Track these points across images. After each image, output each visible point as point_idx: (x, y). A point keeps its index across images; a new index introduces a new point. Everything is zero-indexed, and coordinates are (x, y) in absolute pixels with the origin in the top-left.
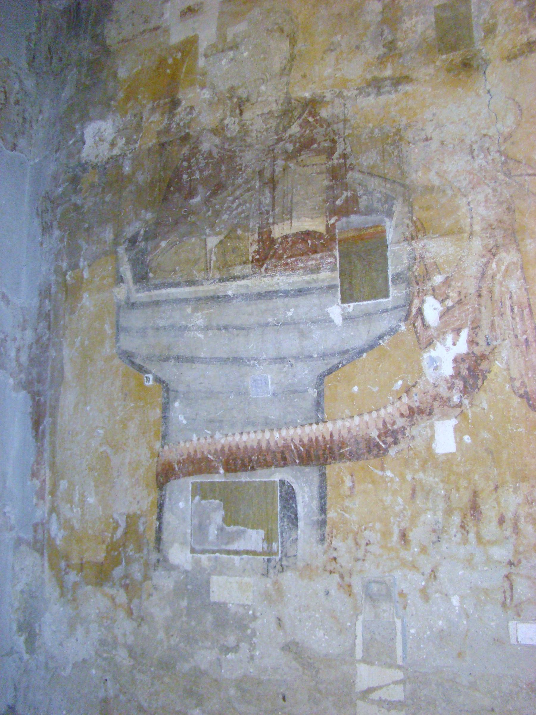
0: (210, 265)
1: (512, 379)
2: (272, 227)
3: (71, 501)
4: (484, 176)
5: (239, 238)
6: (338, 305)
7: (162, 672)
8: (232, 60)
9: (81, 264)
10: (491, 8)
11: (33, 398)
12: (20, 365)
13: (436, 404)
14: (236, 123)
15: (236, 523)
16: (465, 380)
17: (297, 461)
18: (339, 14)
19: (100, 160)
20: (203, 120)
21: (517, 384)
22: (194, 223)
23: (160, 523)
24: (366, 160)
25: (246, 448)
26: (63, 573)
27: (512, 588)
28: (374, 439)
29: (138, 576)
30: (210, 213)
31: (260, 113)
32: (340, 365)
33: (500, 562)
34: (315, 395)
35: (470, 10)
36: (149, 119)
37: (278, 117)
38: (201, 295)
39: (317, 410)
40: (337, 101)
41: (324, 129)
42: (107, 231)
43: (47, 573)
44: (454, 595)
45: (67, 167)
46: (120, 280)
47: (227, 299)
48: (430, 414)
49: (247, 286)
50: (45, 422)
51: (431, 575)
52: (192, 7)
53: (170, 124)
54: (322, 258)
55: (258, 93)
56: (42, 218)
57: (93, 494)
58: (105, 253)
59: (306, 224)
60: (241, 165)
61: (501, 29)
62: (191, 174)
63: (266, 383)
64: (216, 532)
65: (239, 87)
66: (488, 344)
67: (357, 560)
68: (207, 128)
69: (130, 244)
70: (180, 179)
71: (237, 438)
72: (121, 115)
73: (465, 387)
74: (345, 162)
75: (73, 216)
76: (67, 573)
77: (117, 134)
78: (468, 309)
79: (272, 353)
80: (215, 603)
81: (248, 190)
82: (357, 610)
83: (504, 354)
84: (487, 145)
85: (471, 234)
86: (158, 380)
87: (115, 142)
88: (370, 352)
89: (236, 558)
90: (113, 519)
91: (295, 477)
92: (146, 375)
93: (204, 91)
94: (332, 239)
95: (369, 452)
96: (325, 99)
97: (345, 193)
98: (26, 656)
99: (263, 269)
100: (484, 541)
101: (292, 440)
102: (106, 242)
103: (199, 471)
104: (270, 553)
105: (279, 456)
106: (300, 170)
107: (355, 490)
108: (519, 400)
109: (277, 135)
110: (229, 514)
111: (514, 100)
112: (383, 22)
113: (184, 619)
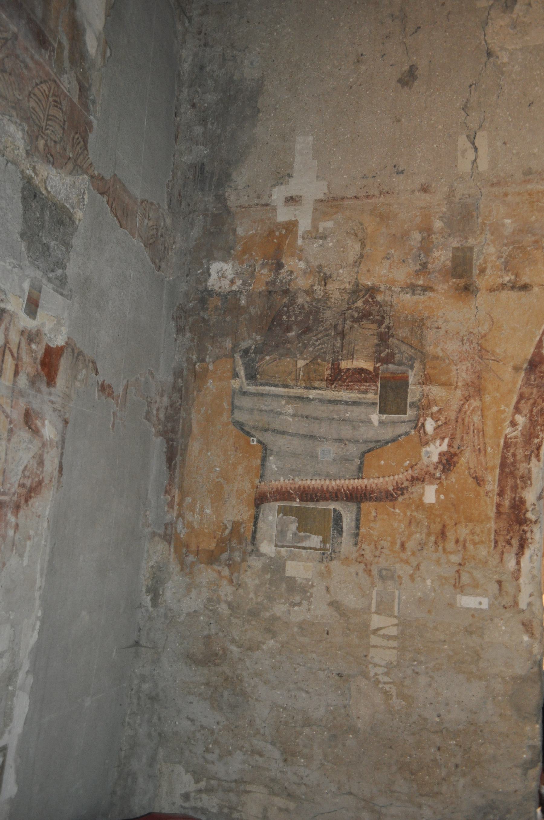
1: (469, 469)
2: (340, 362)
3: (193, 511)
4: (468, 356)
5: (318, 364)
7: (250, 618)
9: (207, 360)
11: (168, 442)
12: (159, 420)
13: (427, 476)
16: (444, 465)
20: (299, 282)
21: (472, 471)
22: (289, 349)
23: (256, 528)
24: (402, 333)
25: (314, 488)
27: (460, 577)
28: (390, 491)
29: (238, 559)
30: (300, 345)
33: (455, 563)
34: (359, 463)
36: (260, 271)
37: (349, 293)
38: (291, 394)
40: (387, 292)
42: (227, 341)
43: (172, 556)
46: (236, 375)
47: (309, 400)
48: (423, 481)
49: (322, 395)
54: (369, 386)
55: (338, 274)
57: (210, 507)
58: (226, 356)
60: (323, 318)
61: (488, 271)
62: (289, 317)
65: (325, 267)
67: (375, 556)
71: (309, 482)
73: (444, 469)
75: (201, 326)
76: (187, 556)
79: (335, 436)
80: (288, 577)
81: (327, 335)
82: (373, 584)
83: (467, 454)
84: (472, 338)
86: (259, 441)
90: (223, 523)
92: (252, 438)
93: (301, 262)
94: (377, 375)
95: (387, 498)
97: (387, 350)
98: (151, 609)
99: (333, 386)
101: (343, 487)
102: (226, 348)
104: (325, 549)
105: (334, 495)
106: (360, 330)
107: (378, 518)
112: (421, 248)
113: (267, 586)
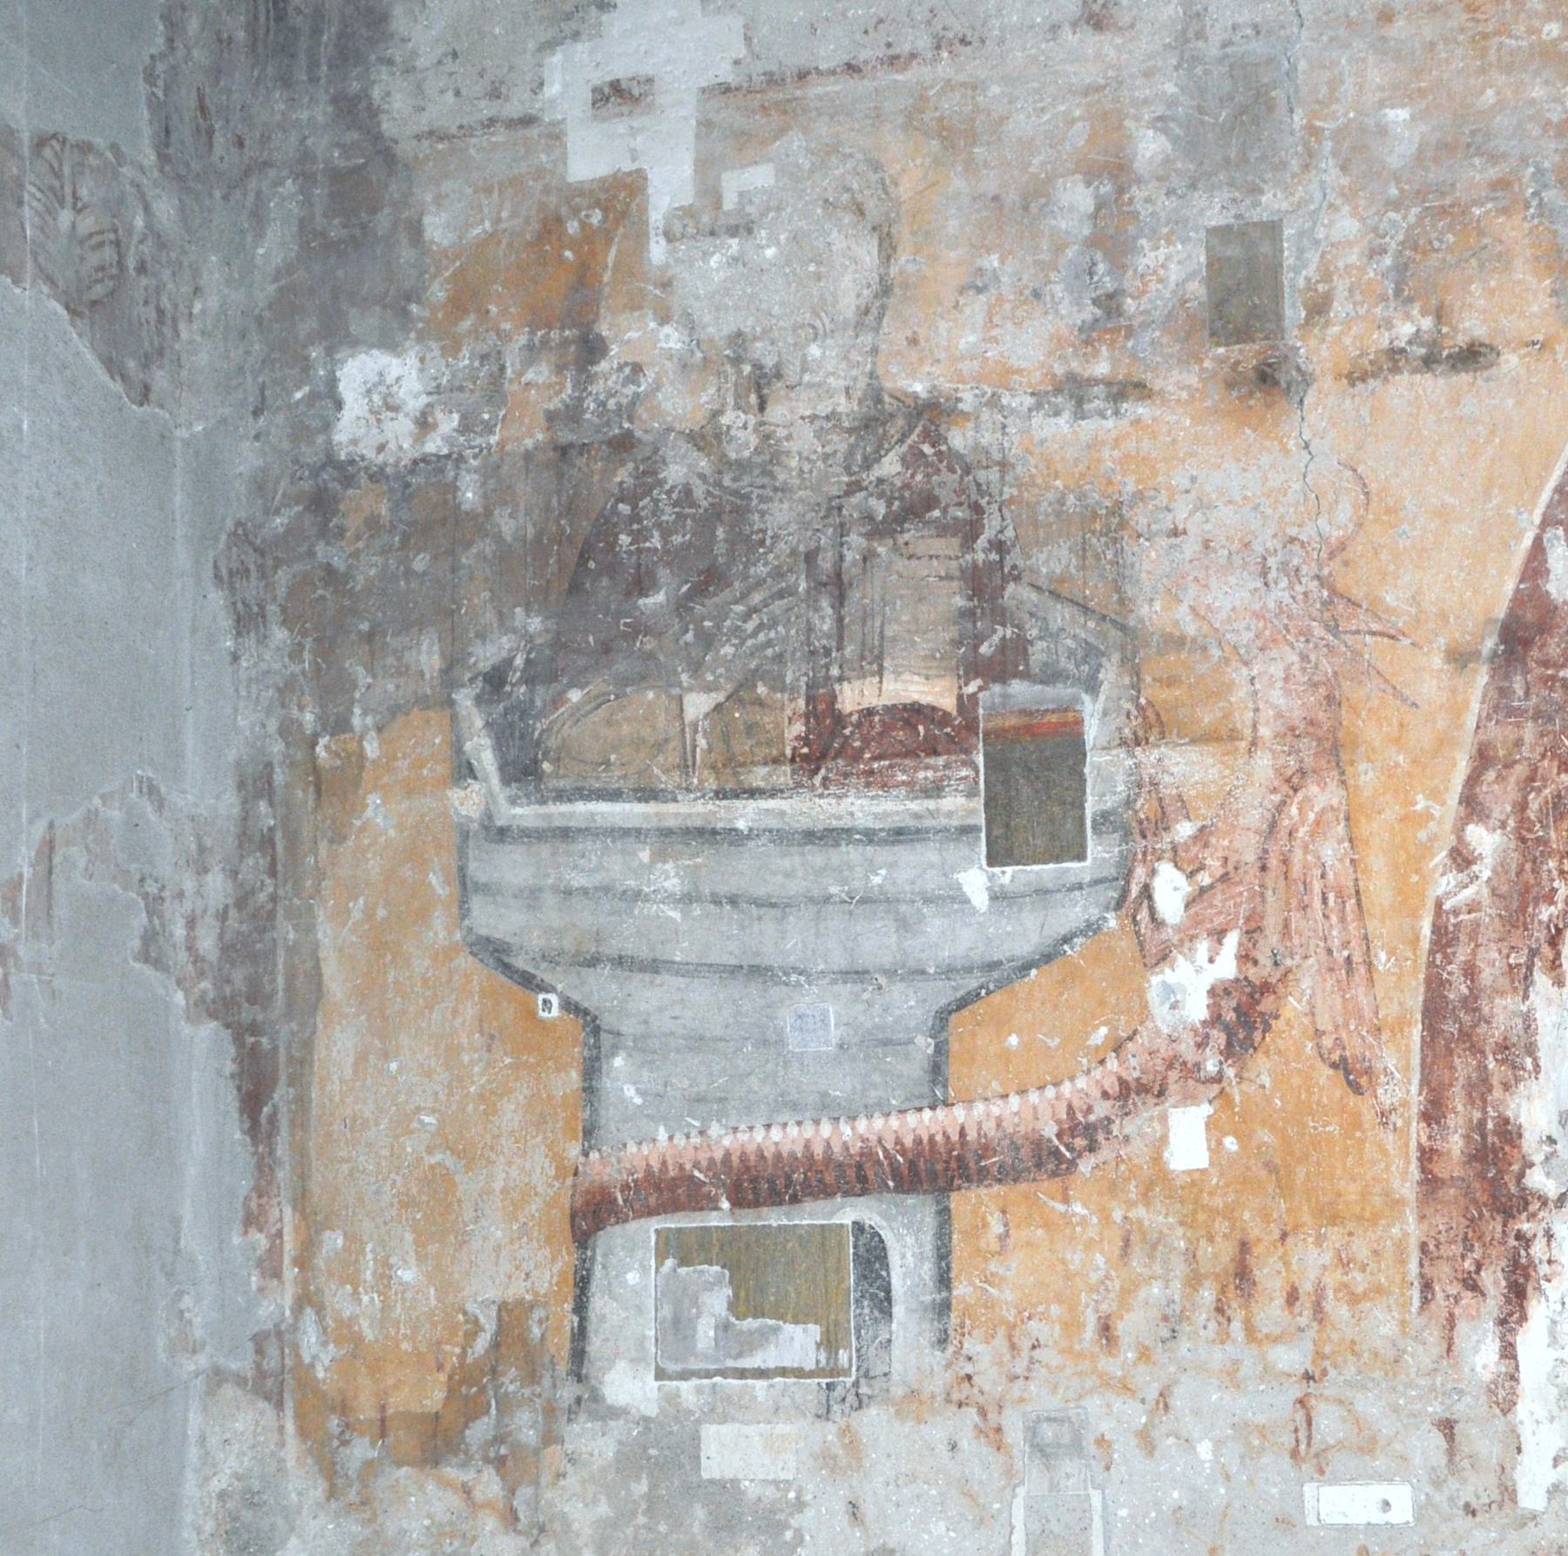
0: (694, 757)
1: (1318, 1034)
2: (837, 687)
4: (1286, 627)
5: (760, 703)
6: (981, 868)
8: (735, 259)
9: (356, 721)
10: (1322, 256)
11: (238, 1040)
12: (197, 959)
13: (1173, 1075)
14: (750, 427)
15: (758, 1313)
16: (1229, 1031)
17: (891, 1184)
18: (996, 198)
19: (391, 461)
20: (667, 406)
21: (1327, 1042)
22: (651, 656)
23: (583, 1320)
24: (1047, 561)
25: (778, 1156)
26: (336, 1443)
27: (1309, 1423)
28: (1049, 1140)
29: (530, 1436)
30: (689, 637)
31: (807, 413)
32: (983, 992)
33: (1289, 1375)
34: (931, 1051)
35: (1282, 251)
36: (521, 374)
37: (850, 431)
38: (671, 823)
39: (934, 1082)
40: (985, 415)
41: (956, 477)
44: (1202, 1439)
45: (296, 461)
46: (465, 771)
47: (735, 838)
48: (1161, 1094)
49: (782, 814)
50: (276, 1096)
51: (1158, 1402)
52: (624, 85)
53: (581, 399)
54: (947, 766)
55: (804, 361)
56: (233, 590)
57: (412, 1259)
58: (423, 702)
59: (913, 688)
60: (764, 531)
61: (1339, 308)
62: (639, 536)
63: (825, 1021)
64: (712, 1333)
65: (755, 339)
66: (1276, 964)
67: (1013, 1378)
68: (678, 427)
69: (488, 687)
70: (612, 545)
71: (759, 1135)
72: (443, 348)
73: (1229, 1044)
74: (1001, 560)
75: (322, 597)
76: (345, 1443)
77: (435, 397)
78: (1241, 894)
79: (839, 961)
80: (712, 1482)
81: (781, 595)
82: (1010, 1475)
83: (1306, 984)
84: (1295, 562)
85: (1254, 744)
86: (568, 1006)
87: (430, 420)
88: (1046, 967)
89: (760, 1384)
90: (465, 1313)
91: (886, 1216)
92: (541, 997)
93: (667, 329)
94: (971, 726)
96: (960, 406)
99: (817, 780)
100: (1259, 1336)
101: (880, 1141)
102: (422, 674)
103: (672, 1206)
106: (900, 564)
107: (1011, 1242)
108: (1331, 1072)
109: (850, 474)
110: (742, 1294)
111: (1355, 470)
112: (1093, 242)
113: (641, 1520)
